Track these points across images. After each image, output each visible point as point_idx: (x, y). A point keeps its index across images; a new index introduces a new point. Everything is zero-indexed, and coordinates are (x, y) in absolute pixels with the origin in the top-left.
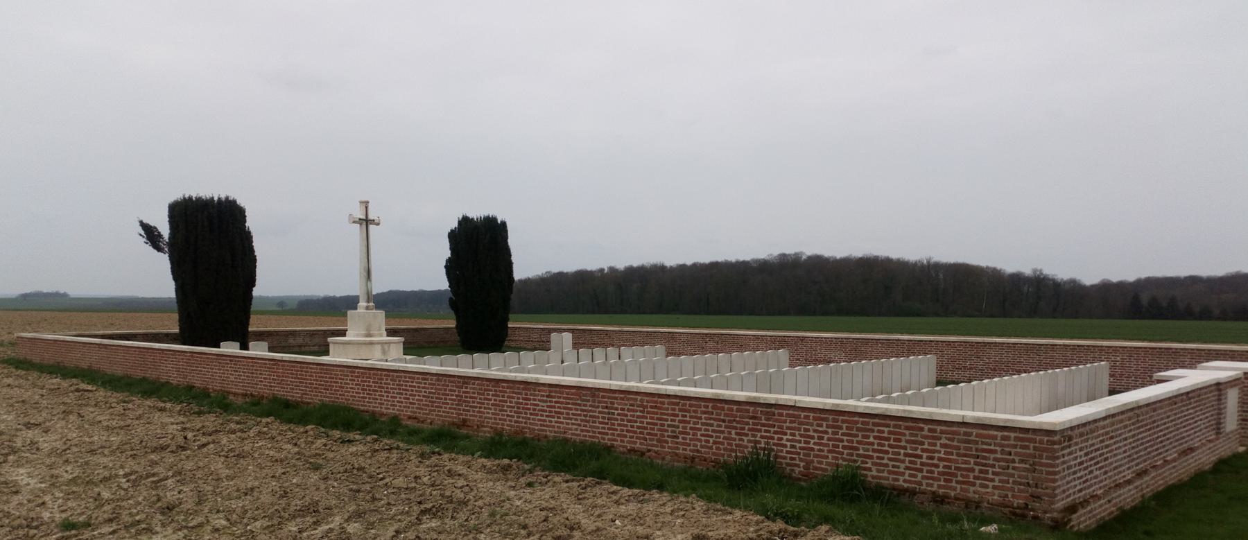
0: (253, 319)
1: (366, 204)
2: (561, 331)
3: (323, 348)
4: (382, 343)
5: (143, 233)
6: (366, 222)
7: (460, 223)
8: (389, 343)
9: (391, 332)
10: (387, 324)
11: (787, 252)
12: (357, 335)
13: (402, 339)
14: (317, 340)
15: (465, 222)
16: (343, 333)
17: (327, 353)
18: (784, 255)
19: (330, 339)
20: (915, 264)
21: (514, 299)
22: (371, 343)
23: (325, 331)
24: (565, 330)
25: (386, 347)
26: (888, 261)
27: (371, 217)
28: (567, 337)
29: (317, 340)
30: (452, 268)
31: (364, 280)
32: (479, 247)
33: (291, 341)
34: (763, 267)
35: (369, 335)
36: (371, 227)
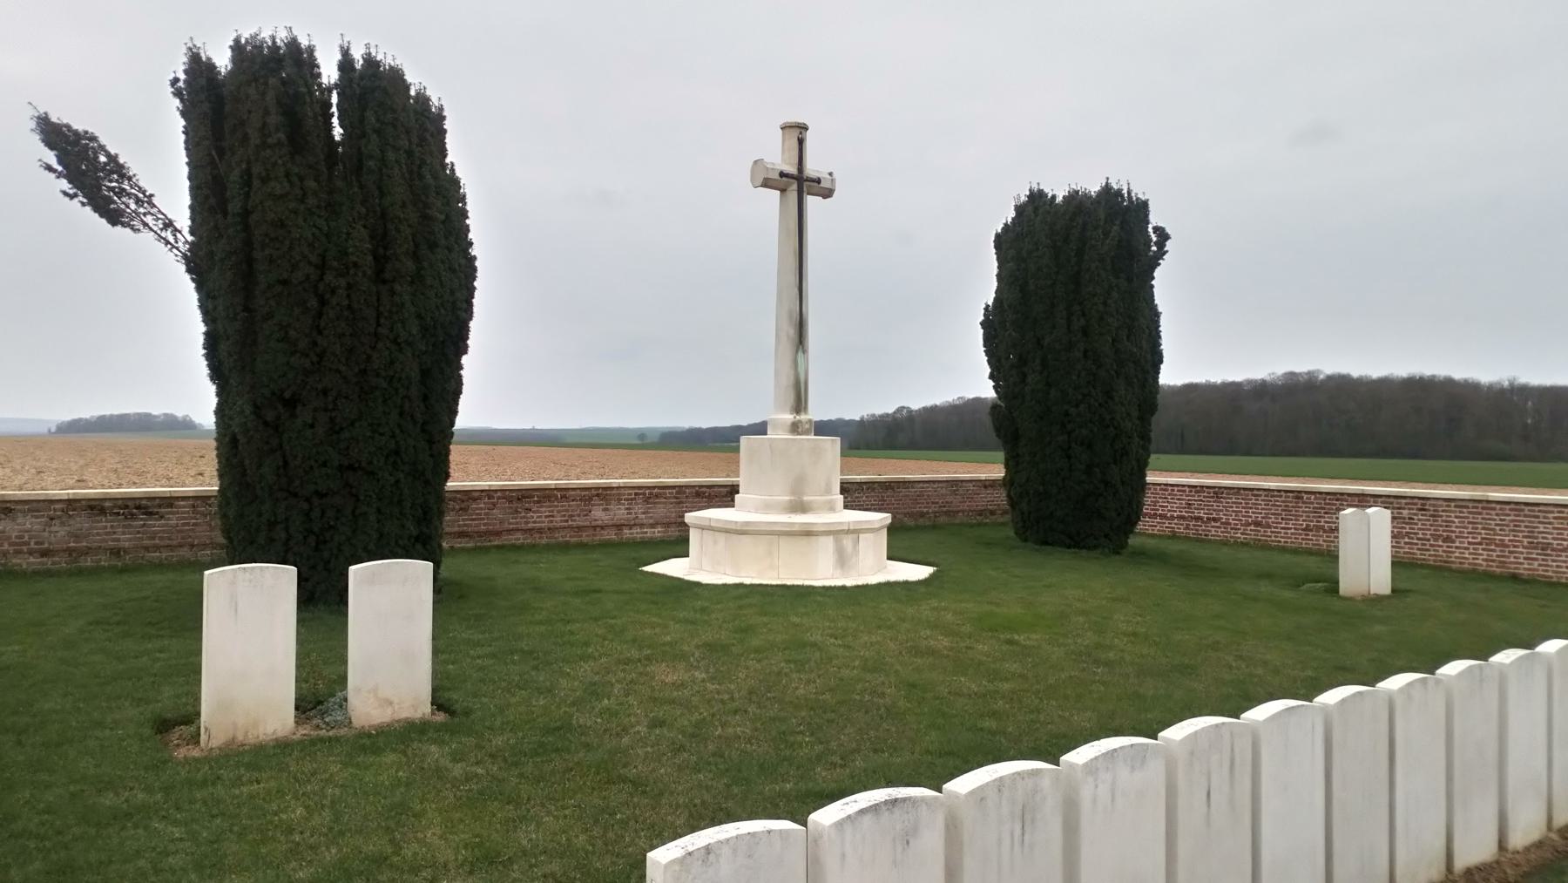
0: (456, 454)
1: (797, 132)
2: (1363, 500)
3: (673, 532)
4: (837, 533)
5: (51, 158)
6: (799, 185)
7: (1020, 209)
8: (855, 532)
9: (855, 495)
10: (842, 473)
11: (1297, 370)
12: (767, 507)
13: (882, 518)
14: (661, 510)
15: (1036, 203)
16: (726, 495)
17: (679, 546)
18: (1292, 374)
19: (690, 517)
20: (1490, 387)
21: (1160, 422)
22: (808, 533)
23: (680, 489)
24: (1375, 499)
25: (847, 542)
26: (1449, 382)
27: (813, 167)
28: (1380, 517)
29: (661, 510)
30: (1005, 333)
31: (787, 348)
32: (1075, 278)
33: (598, 514)
34: (1260, 391)
35: (800, 507)
36: (811, 201)
